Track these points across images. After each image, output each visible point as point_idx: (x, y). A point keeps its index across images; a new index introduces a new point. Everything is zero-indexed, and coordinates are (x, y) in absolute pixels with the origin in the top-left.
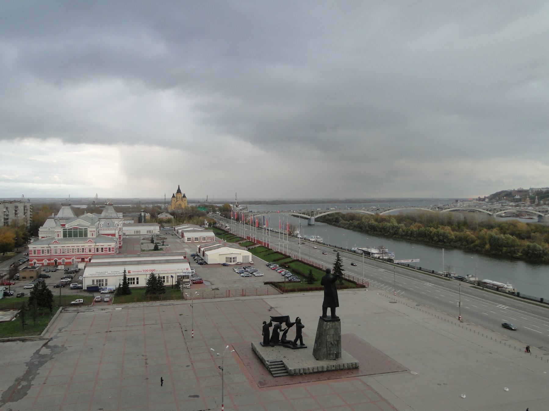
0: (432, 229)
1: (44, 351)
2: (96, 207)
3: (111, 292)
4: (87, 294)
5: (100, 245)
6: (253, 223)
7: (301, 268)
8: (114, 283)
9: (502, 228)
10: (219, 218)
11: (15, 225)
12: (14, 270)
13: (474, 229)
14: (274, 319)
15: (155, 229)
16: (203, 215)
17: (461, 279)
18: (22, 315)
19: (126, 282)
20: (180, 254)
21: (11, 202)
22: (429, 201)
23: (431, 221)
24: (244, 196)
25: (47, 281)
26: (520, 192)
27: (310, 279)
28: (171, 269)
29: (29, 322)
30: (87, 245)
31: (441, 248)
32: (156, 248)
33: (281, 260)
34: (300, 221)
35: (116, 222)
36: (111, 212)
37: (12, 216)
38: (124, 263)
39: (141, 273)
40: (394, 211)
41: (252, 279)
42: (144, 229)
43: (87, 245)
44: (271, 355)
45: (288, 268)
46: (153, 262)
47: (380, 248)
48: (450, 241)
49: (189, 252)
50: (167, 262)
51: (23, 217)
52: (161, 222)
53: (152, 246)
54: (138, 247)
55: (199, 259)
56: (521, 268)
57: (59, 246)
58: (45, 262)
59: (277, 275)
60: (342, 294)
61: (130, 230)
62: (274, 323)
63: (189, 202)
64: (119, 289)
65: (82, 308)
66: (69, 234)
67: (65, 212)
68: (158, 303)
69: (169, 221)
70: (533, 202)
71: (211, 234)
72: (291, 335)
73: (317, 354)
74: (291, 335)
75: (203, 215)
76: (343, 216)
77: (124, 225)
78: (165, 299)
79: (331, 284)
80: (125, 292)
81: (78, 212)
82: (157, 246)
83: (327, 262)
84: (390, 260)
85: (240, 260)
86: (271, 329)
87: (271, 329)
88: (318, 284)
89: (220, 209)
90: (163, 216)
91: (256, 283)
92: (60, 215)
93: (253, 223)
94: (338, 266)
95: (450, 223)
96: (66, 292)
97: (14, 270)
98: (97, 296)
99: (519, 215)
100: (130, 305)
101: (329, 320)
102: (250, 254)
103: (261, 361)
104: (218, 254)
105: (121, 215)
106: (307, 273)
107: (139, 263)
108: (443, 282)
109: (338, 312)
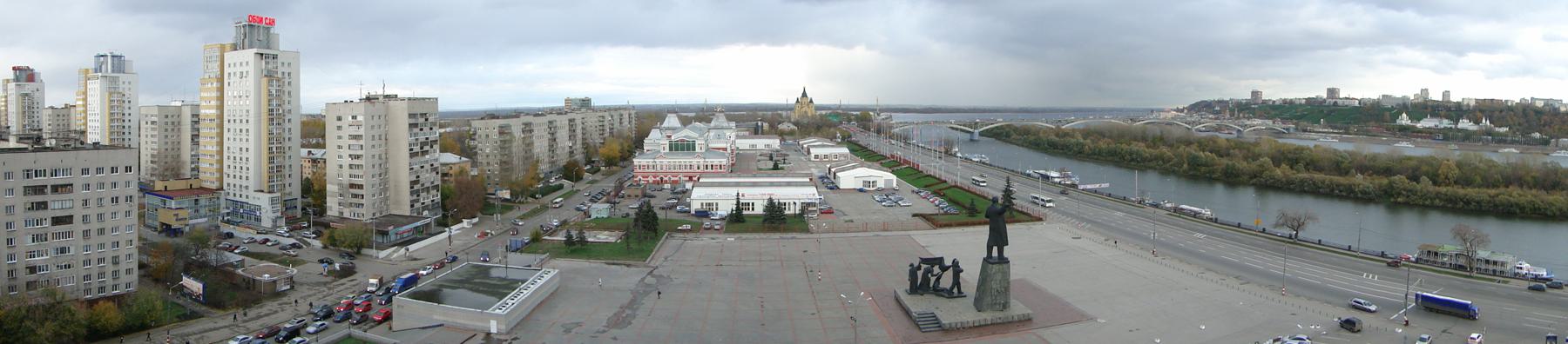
0: (1124, 146)
1: (649, 280)
2: (704, 115)
3: (723, 219)
4: (695, 219)
5: (709, 161)
6: (898, 137)
7: (960, 197)
8: (725, 208)
9: (1202, 145)
10: (855, 128)
11: (620, 136)
12: (619, 187)
13: (1171, 146)
14: (924, 261)
15: (775, 143)
16: (835, 126)
17: (1156, 206)
18: (627, 236)
19: (740, 207)
20: (806, 175)
21: (617, 109)
22: (1120, 111)
23: (1121, 135)
24: (886, 101)
25: (653, 202)
26: (1220, 102)
27: (972, 211)
28: (795, 194)
29: (634, 246)
30: (695, 161)
31: (1133, 169)
32: (776, 167)
33: (935, 186)
34: (959, 134)
35: (728, 133)
36: (721, 120)
37: (617, 125)
38: (737, 185)
39: (757, 197)
40: (1078, 123)
41: (898, 209)
42: (761, 143)
43: (695, 161)
44: (918, 305)
45: (943, 196)
46: (772, 184)
47: (1061, 171)
48: (1145, 160)
49: (816, 172)
50: (789, 184)
51: (628, 127)
52: (782, 135)
53: (771, 164)
54: (753, 166)
55: (828, 182)
56: (1219, 190)
57: (665, 161)
58: (651, 179)
59: (930, 205)
60: (1011, 229)
61: (745, 144)
62: (924, 266)
63: (819, 108)
64: (731, 215)
65: (691, 236)
66: (685, 147)
67: (672, 121)
68: (777, 235)
69: (791, 133)
70: (1232, 115)
71: (845, 150)
72: (947, 281)
73: (979, 305)
74: (947, 281)
75: (835, 126)
76: (1016, 129)
77: (738, 137)
78: (786, 230)
79: (999, 217)
80: (738, 219)
81: (686, 122)
82: (777, 164)
83: (992, 188)
84: (1074, 186)
85: (881, 184)
86: (920, 274)
87: (920, 274)
88: (982, 217)
89: (858, 118)
90: (784, 127)
91: (902, 214)
92: (665, 124)
93: (898, 137)
94: (1008, 193)
95: (1144, 139)
96: (672, 215)
97: (619, 187)
98: (707, 223)
99: (1219, 129)
100: (744, 236)
101: (995, 260)
102: (894, 177)
103: (907, 312)
104: (851, 178)
105: (733, 124)
106: (967, 203)
107: (754, 185)
108: (1136, 210)
109: (1007, 252)
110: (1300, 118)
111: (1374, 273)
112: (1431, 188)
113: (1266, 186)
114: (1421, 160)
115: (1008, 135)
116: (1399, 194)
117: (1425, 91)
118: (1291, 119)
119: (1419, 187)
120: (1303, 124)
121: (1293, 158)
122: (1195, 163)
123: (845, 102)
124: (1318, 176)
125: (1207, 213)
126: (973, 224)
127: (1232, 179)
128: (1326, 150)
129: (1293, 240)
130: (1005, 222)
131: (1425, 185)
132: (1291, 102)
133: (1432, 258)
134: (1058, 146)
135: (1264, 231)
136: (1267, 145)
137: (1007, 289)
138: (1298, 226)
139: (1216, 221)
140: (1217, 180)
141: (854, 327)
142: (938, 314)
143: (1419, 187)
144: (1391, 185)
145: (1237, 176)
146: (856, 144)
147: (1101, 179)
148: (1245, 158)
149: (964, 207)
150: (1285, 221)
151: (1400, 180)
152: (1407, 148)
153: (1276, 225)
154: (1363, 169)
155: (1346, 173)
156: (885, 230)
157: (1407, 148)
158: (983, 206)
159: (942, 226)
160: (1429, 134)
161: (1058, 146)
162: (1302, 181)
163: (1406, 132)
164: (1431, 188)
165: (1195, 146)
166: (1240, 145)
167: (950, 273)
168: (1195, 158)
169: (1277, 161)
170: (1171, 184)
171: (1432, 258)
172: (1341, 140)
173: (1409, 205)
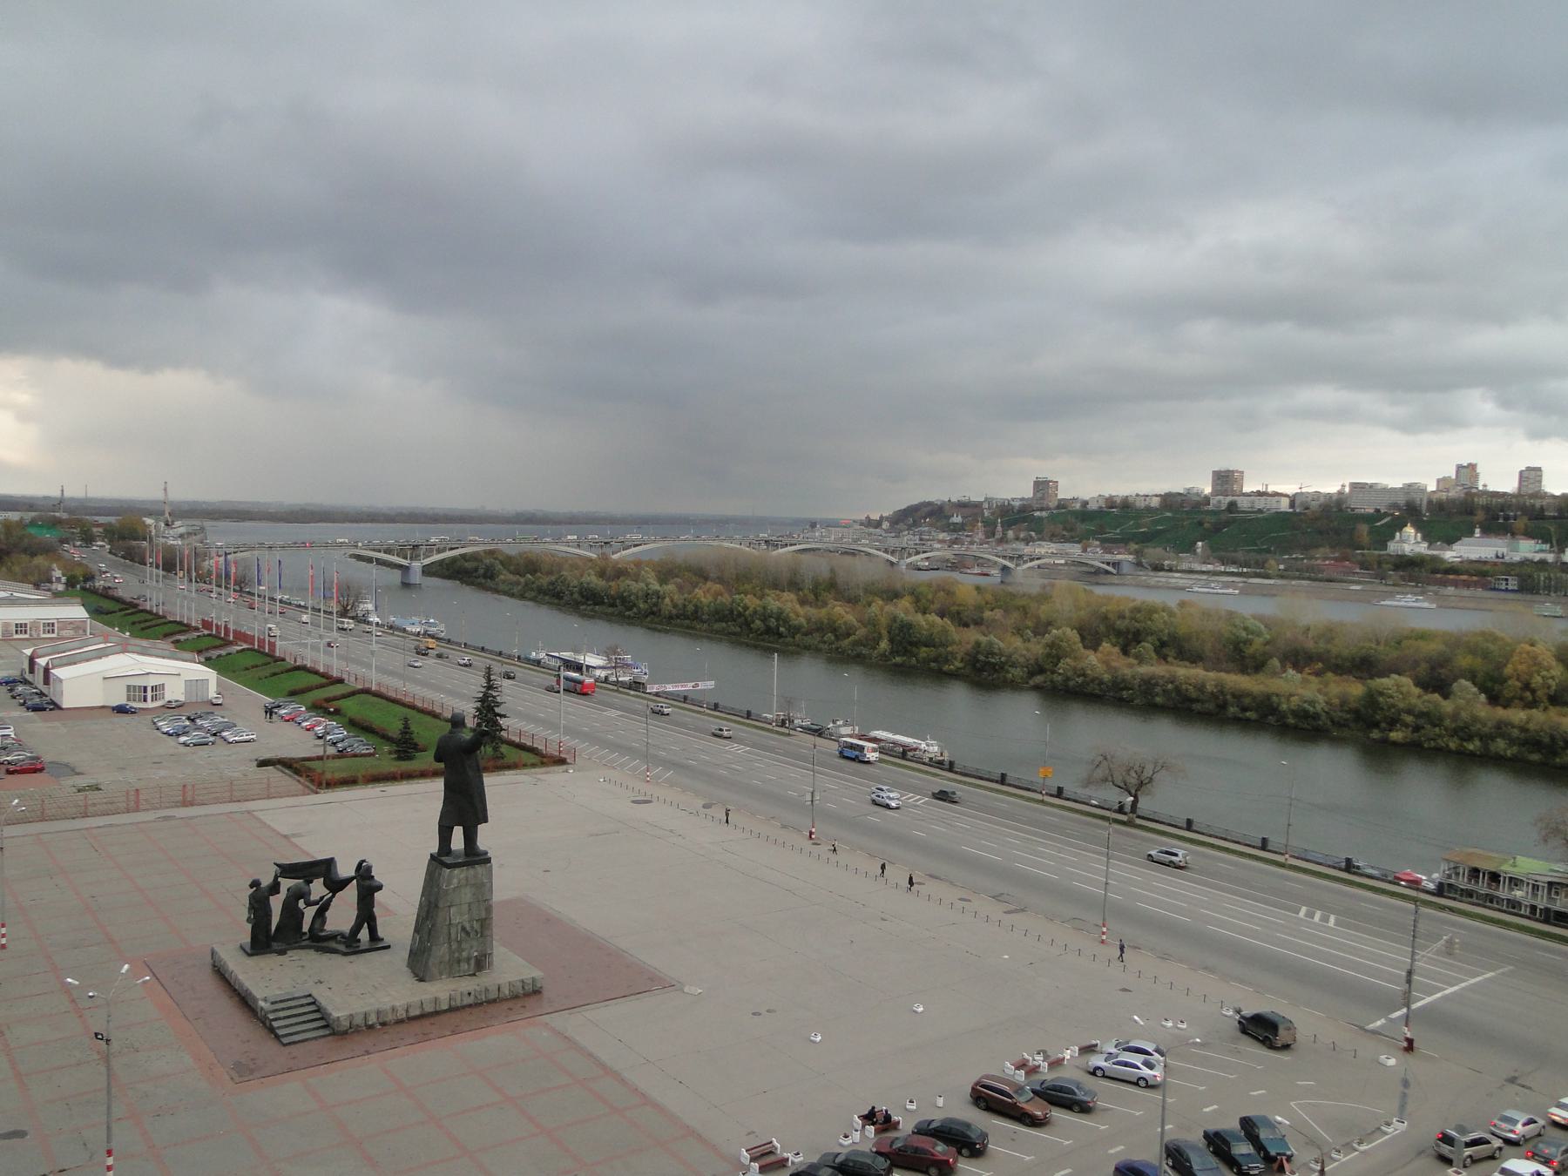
0: (752, 602)
6: (224, 578)
13: (852, 601)
14: (288, 870)
17: (819, 732)
23: (742, 577)
24: (185, 492)
26: (962, 506)
27: (405, 746)
31: (771, 651)
33: (319, 692)
34: (373, 569)
41: (220, 751)
47: (609, 652)
56: (959, 697)
59: (300, 736)
60: (496, 786)
62: (286, 884)
71: (77, 612)
74: (342, 914)
75: (47, 550)
76: (507, 562)
79: (468, 761)
83: (451, 692)
86: (276, 903)
87: (276, 903)
88: (426, 760)
89: (111, 534)
91: (228, 764)
93: (224, 578)
94: (488, 707)
95: (794, 585)
99: (957, 565)
102: (209, 675)
103: (244, 1001)
106: (394, 728)
108: (773, 740)
109: (486, 837)
110: (1147, 538)
111: (1328, 909)
112: (1483, 710)
113: (1068, 692)
114: (1456, 642)
115: (490, 574)
116: (1393, 723)
117: (1468, 471)
118: (1124, 541)
119: (1447, 706)
120: (1154, 552)
121: (1129, 634)
122: (904, 639)
123: (74, 491)
124: (1186, 673)
125: (931, 748)
126: (408, 776)
127: (985, 674)
128: (1206, 614)
129: (1128, 816)
130: (480, 771)
131: (1468, 701)
132: (930, 504)
133: (1482, 887)
134: (604, 599)
135: (1059, 793)
136: (1069, 601)
137: (485, 923)
138: (1139, 786)
139: (951, 767)
140: (954, 676)
141: (107, 1059)
142: (325, 998)
143: (1447, 706)
144: (1371, 699)
145: (998, 668)
146: (106, 594)
147: (702, 669)
148: (1019, 631)
149: (392, 741)
150: (1104, 771)
151: (1400, 688)
152: (1414, 612)
153: (1088, 782)
154: (1298, 658)
155: (1255, 665)
156: (186, 803)
157: (1414, 612)
158: (429, 734)
159: (331, 785)
160: (1480, 575)
161: (604, 599)
162: (1148, 684)
163: (1412, 570)
164: (1483, 710)
165: (906, 602)
166: (1005, 601)
167: (350, 894)
168: (906, 627)
169: (1091, 638)
170: (853, 684)
171: (1482, 887)
172: (1246, 591)
173: (1417, 750)
